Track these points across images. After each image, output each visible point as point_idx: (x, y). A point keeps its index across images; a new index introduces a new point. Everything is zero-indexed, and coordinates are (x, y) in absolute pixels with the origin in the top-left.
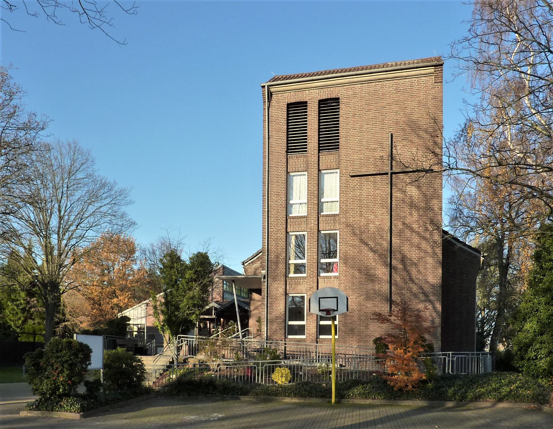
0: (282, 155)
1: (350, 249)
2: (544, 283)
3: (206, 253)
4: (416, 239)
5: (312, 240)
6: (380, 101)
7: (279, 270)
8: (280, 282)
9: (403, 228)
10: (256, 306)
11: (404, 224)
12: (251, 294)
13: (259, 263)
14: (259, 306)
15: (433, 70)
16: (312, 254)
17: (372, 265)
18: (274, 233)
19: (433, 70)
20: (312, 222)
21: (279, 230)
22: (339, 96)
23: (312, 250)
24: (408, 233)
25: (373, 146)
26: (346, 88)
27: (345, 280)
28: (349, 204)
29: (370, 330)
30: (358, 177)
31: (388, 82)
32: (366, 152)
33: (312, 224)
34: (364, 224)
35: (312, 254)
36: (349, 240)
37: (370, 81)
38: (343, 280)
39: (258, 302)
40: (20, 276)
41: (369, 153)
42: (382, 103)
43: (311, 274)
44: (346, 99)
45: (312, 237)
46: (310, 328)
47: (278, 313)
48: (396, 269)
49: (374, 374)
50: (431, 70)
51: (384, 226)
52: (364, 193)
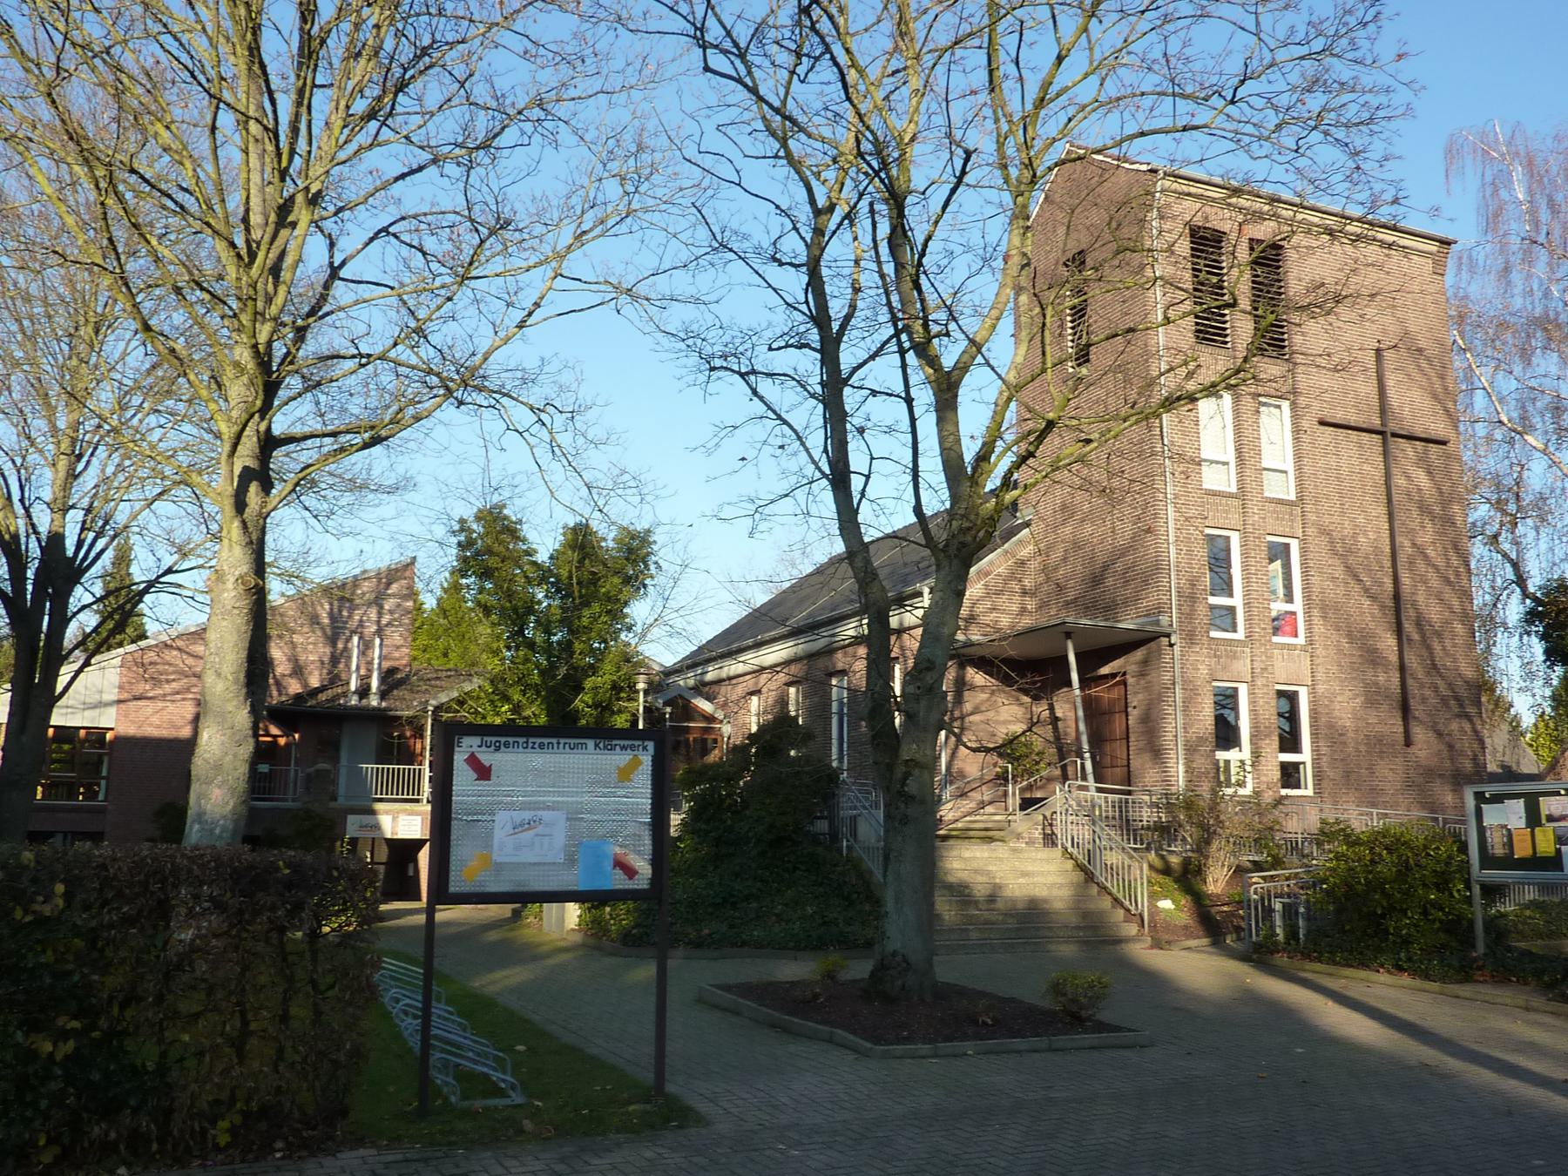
2: (1416, 865)
3: (520, 522)
4: (1435, 582)
11: (1414, 545)
13: (979, 586)
14: (983, 702)
15: (1435, 248)
19: (1435, 248)
24: (1421, 565)
48: (1410, 640)
49: (675, 819)
50: (1433, 247)
52: (1344, 463)
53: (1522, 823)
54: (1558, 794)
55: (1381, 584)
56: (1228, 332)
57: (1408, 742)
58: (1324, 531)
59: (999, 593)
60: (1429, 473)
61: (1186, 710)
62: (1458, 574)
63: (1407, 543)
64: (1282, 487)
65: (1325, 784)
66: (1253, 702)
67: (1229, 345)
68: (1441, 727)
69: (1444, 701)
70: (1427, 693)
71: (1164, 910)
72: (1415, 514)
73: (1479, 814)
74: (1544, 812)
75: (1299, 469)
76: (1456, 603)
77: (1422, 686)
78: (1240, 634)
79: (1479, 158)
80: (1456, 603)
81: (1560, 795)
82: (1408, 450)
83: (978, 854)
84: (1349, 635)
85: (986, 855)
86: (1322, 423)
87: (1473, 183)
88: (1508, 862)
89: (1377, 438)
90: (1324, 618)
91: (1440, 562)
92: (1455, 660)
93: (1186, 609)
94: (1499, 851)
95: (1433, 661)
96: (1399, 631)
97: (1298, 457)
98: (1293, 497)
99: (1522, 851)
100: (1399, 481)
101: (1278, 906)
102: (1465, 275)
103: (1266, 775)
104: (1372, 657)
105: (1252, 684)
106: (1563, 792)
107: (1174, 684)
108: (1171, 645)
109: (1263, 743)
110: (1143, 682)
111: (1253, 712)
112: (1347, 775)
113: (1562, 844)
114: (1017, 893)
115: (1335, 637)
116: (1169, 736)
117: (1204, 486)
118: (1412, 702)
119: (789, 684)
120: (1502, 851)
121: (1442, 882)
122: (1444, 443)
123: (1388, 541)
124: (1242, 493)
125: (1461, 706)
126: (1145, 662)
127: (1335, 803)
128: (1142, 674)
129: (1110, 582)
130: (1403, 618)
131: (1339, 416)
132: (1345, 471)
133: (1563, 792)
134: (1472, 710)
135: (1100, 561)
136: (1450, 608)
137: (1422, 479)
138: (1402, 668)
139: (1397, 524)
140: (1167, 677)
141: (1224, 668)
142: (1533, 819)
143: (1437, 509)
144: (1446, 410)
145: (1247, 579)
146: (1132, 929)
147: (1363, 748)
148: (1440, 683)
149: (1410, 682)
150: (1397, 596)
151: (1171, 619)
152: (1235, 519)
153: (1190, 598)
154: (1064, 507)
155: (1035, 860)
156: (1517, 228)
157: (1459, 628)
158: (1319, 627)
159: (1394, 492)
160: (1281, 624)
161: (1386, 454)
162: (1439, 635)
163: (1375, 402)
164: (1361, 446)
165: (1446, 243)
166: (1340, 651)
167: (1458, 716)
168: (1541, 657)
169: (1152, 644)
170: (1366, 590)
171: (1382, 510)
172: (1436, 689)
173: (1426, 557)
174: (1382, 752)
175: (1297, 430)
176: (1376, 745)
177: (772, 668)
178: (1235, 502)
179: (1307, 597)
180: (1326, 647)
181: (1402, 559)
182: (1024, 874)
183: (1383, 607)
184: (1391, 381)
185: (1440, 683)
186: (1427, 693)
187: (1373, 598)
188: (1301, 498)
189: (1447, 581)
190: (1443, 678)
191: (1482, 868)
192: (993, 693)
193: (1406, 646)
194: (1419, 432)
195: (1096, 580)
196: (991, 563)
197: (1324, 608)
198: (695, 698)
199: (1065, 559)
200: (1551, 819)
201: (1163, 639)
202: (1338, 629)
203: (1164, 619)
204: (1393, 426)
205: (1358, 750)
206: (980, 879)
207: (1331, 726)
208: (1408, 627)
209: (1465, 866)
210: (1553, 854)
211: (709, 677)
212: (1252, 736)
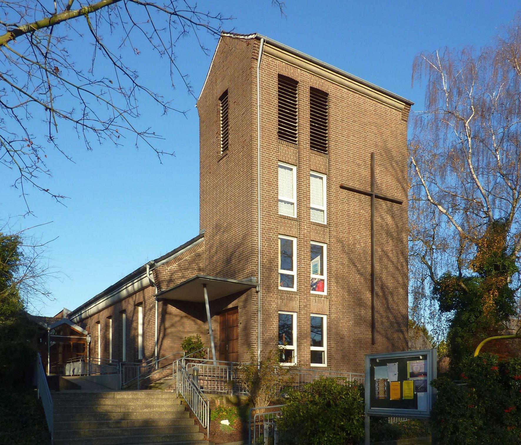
0: (274, 136)
1: (340, 267)
4: (391, 269)
5: (305, 249)
6: (363, 116)
7: (272, 280)
8: (273, 295)
9: (382, 255)
10: (173, 321)
11: (383, 251)
12: (166, 305)
13: (175, 265)
14: (176, 322)
16: (306, 266)
17: (359, 289)
18: (265, 231)
19: (403, 107)
20: (305, 228)
21: (271, 228)
22: (329, 91)
23: (305, 261)
24: (385, 260)
25: (358, 161)
26: (335, 87)
27: (336, 301)
28: (339, 217)
29: (358, 358)
30: (346, 191)
31: (369, 100)
32: (352, 165)
33: (306, 230)
34: (351, 242)
35: (306, 266)
36: (339, 257)
37: (356, 91)
38: (335, 301)
39: (174, 317)
40: (449, 220)
41: (355, 168)
42: (364, 119)
43: (305, 290)
44: (335, 99)
45: (305, 245)
46: (304, 354)
47: (272, 334)
48: (377, 295)
50: (402, 106)
51: (368, 249)
52: (351, 208)
53: (395, 378)
54: (418, 359)
55: (366, 268)
56: (297, 135)
57: (373, 343)
58: (339, 241)
59: (187, 269)
60: (393, 217)
61: (264, 324)
62: (402, 266)
63: (379, 250)
64: (322, 219)
65: (333, 361)
66: (299, 322)
67: (297, 143)
68: (389, 336)
69: (392, 324)
70: (384, 320)
71: (224, 426)
72: (384, 236)
73: (372, 373)
74: (409, 370)
75: (329, 209)
76: (400, 279)
77: (382, 317)
78: (295, 289)
79: (428, 68)
80: (400, 279)
81: (420, 359)
82: (384, 205)
83: (125, 397)
84: (349, 292)
85: (131, 397)
86: (342, 187)
87: (425, 81)
88: (387, 403)
89: (368, 198)
90: (337, 283)
91: (394, 260)
92: (398, 306)
93: (266, 274)
94: (382, 396)
95: (388, 306)
96: (372, 291)
97: (329, 203)
98: (325, 223)
99: (394, 396)
100: (378, 219)
101: (266, 426)
102: (418, 129)
103: (304, 357)
104: (359, 302)
105: (299, 314)
106: (421, 357)
107: (258, 311)
108: (257, 292)
109: (302, 341)
110: (244, 311)
111: (299, 326)
112: (344, 357)
113: (418, 391)
114: (139, 417)
115: (341, 291)
116: (254, 337)
117: (279, 213)
118: (376, 324)
119: (109, 317)
120: (383, 396)
121: (348, 413)
122: (400, 203)
123: (370, 248)
124: (299, 220)
125: (399, 326)
126: (246, 301)
127: (337, 370)
128: (244, 307)
129: (233, 261)
130: (375, 284)
131: (351, 185)
132: (351, 212)
133: (421, 357)
134: (404, 329)
135: (230, 250)
136: (398, 281)
137: (389, 219)
138: (373, 308)
139: (375, 239)
140: (254, 307)
141: (286, 305)
142: (403, 375)
143: (395, 234)
144: (403, 188)
145: (299, 262)
146: (201, 436)
147: (352, 345)
148: (390, 316)
149: (376, 315)
150: (372, 275)
151: (258, 279)
152: (295, 231)
153: (269, 268)
154: (217, 226)
155: (162, 399)
156: (443, 105)
157: (401, 291)
158: (334, 287)
159: (374, 225)
160: (318, 286)
161: (372, 205)
162: (392, 294)
163: (369, 180)
164: (360, 201)
165: (408, 104)
166: (343, 299)
167: (398, 331)
168: (438, 308)
169: (249, 292)
170: (358, 271)
171: (369, 233)
172: (388, 318)
173: (388, 256)
174: (361, 347)
175: (329, 187)
176: (359, 343)
177: (103, 309)
178: (296, 223)
179: (329, 272)
180: (337, 297)
181: (376, 256)
182: (147, 407)
183: (365, 279)
184: (377, 171)
185: (390, 316)
186: (384, 320)
187: (361, 274)
188: (329, 224)
189: (397, 268)
190: (392, 313)
191: (372, 406)
192: (182, 317)
193: (375, 298)
194: (389, 196)
195: (228, 261)
196: (182, 254)
197: (337, 278)
198: (72, 325)
199: (216, 253)
200: (413, 375)
201: (253, 289)
202: (343, 288)
203: (254, 279)
204: (376, 192)
205: (349, 346)
206: (119, 410)
207: (337, 334)
208: (376, 288)
209: (362, 406)
210: (412, 398)
211: (83, 316)
212: (298, 338)
